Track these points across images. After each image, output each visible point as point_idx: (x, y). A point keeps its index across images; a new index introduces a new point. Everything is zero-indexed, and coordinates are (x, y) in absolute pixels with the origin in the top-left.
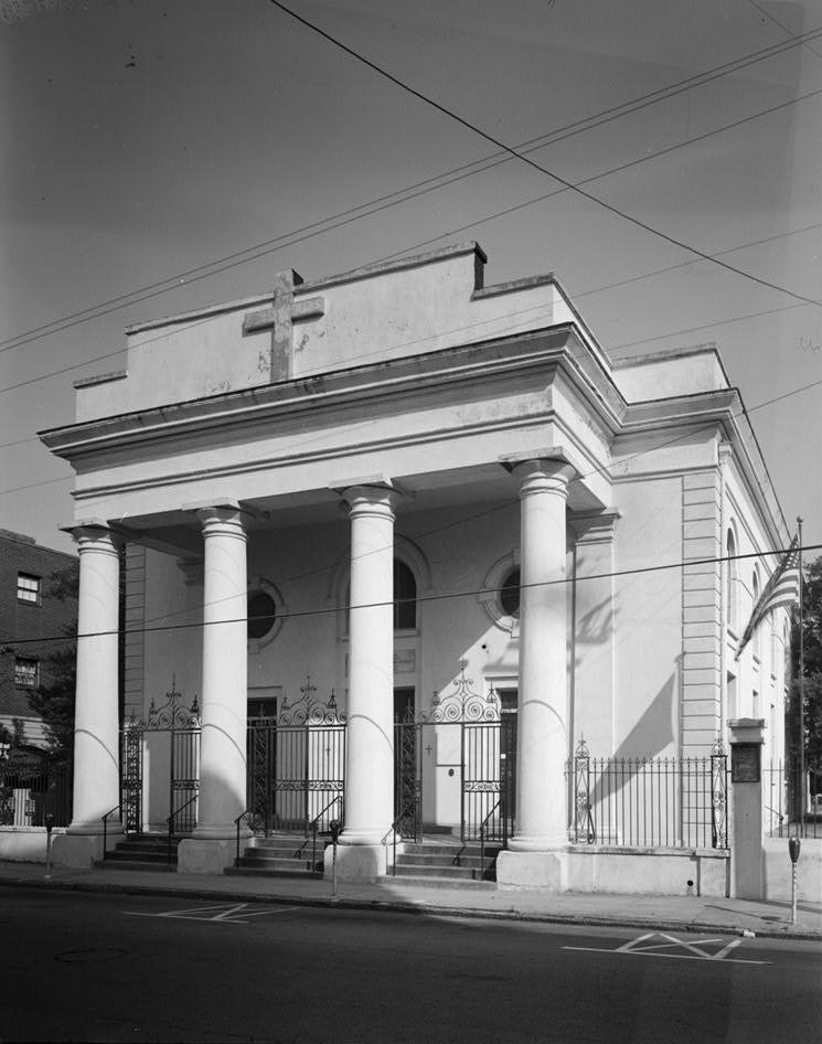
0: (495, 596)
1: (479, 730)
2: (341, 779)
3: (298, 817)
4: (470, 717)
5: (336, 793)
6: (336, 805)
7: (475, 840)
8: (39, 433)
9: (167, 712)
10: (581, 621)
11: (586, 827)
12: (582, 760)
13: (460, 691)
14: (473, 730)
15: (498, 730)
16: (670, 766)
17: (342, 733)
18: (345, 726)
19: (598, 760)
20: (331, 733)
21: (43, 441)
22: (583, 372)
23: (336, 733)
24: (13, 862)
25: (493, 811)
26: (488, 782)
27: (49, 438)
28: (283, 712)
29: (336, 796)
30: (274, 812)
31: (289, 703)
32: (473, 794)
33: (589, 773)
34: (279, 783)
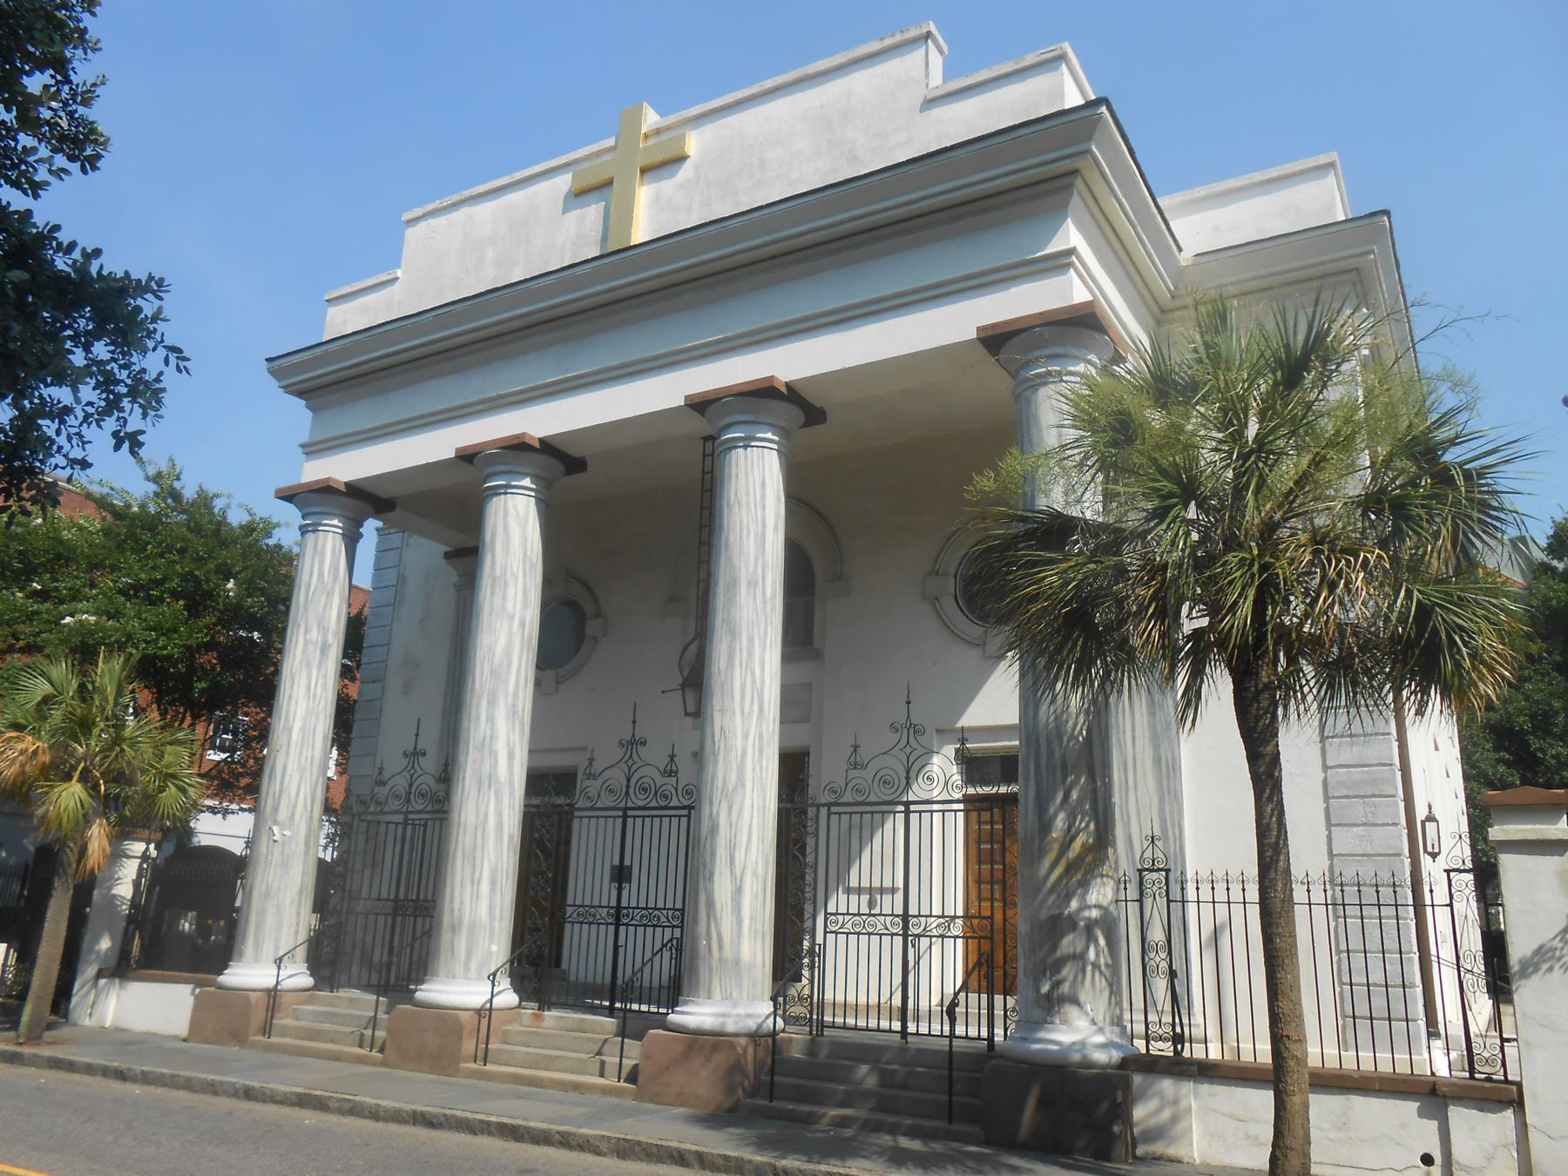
0: (950, 584)
1: (926, 816)
2: (679, 905)
3: (599, 980)
4: (638, 800)
5: (668, 931)
6: (666, 955)
7: (979, 1038)
8: (269, 360)
9: (400, 784)
10: (330, 645)
11: (1167, 1019)
12: (1155, 875)
13: (902, 745)
14: (639, 821)
15: (961, 815)
16: (1220, 888)
17: (684, 821)
18: (690, 808)
19: (1204, 874)
20: (657, 821)
21: (272, 372)
22: (1119, 210)
23: (675, 821)
24: (1322, 1086)
25: (651, 960)
26: (592, 907)
27: (280, 367)
28: (587, 783)
29: (667, 937)
30: (558, 963)
31: (597, 768)
32: (841, 938)
33: (1169, 901)
34: (569, 910)
